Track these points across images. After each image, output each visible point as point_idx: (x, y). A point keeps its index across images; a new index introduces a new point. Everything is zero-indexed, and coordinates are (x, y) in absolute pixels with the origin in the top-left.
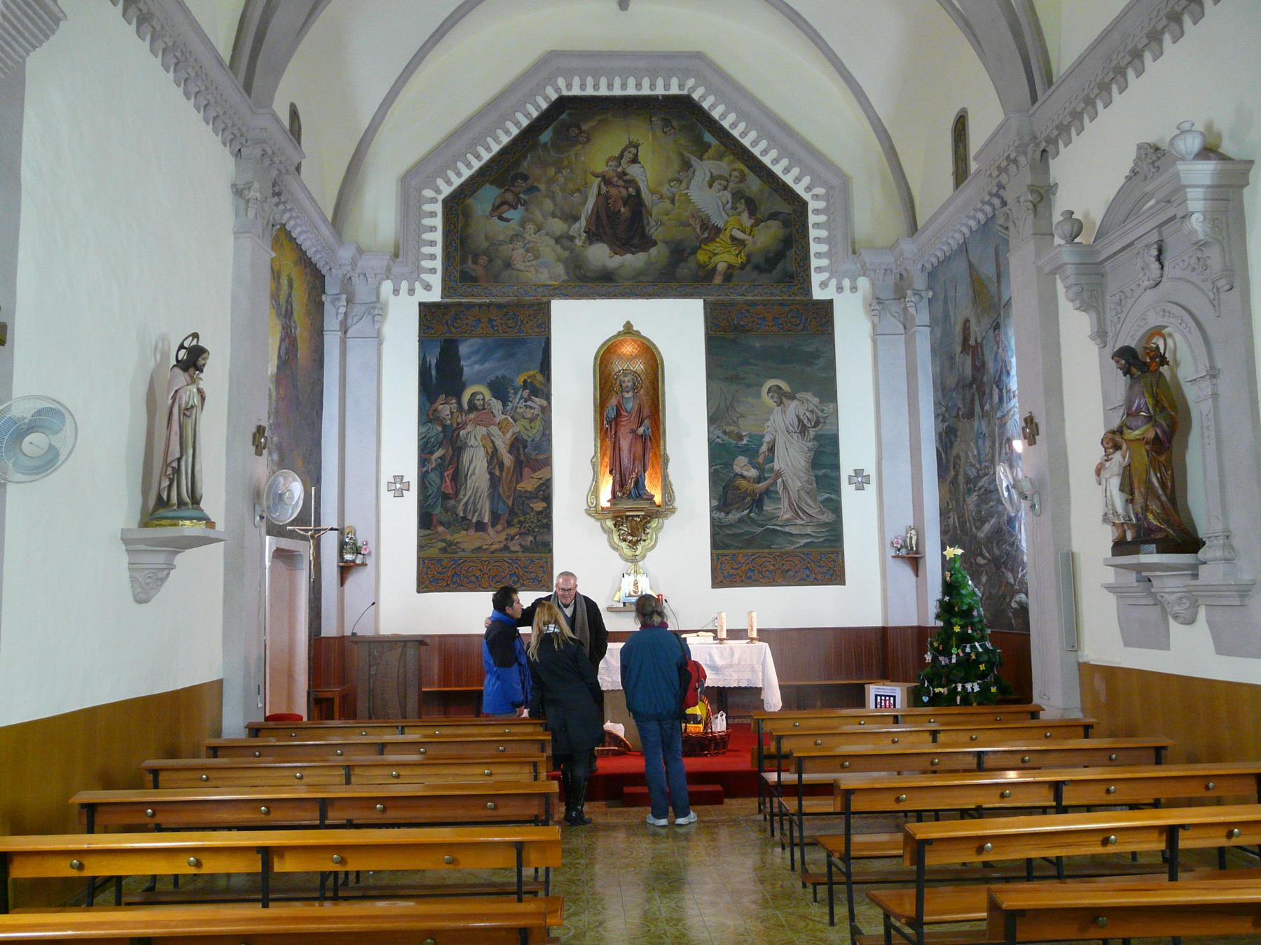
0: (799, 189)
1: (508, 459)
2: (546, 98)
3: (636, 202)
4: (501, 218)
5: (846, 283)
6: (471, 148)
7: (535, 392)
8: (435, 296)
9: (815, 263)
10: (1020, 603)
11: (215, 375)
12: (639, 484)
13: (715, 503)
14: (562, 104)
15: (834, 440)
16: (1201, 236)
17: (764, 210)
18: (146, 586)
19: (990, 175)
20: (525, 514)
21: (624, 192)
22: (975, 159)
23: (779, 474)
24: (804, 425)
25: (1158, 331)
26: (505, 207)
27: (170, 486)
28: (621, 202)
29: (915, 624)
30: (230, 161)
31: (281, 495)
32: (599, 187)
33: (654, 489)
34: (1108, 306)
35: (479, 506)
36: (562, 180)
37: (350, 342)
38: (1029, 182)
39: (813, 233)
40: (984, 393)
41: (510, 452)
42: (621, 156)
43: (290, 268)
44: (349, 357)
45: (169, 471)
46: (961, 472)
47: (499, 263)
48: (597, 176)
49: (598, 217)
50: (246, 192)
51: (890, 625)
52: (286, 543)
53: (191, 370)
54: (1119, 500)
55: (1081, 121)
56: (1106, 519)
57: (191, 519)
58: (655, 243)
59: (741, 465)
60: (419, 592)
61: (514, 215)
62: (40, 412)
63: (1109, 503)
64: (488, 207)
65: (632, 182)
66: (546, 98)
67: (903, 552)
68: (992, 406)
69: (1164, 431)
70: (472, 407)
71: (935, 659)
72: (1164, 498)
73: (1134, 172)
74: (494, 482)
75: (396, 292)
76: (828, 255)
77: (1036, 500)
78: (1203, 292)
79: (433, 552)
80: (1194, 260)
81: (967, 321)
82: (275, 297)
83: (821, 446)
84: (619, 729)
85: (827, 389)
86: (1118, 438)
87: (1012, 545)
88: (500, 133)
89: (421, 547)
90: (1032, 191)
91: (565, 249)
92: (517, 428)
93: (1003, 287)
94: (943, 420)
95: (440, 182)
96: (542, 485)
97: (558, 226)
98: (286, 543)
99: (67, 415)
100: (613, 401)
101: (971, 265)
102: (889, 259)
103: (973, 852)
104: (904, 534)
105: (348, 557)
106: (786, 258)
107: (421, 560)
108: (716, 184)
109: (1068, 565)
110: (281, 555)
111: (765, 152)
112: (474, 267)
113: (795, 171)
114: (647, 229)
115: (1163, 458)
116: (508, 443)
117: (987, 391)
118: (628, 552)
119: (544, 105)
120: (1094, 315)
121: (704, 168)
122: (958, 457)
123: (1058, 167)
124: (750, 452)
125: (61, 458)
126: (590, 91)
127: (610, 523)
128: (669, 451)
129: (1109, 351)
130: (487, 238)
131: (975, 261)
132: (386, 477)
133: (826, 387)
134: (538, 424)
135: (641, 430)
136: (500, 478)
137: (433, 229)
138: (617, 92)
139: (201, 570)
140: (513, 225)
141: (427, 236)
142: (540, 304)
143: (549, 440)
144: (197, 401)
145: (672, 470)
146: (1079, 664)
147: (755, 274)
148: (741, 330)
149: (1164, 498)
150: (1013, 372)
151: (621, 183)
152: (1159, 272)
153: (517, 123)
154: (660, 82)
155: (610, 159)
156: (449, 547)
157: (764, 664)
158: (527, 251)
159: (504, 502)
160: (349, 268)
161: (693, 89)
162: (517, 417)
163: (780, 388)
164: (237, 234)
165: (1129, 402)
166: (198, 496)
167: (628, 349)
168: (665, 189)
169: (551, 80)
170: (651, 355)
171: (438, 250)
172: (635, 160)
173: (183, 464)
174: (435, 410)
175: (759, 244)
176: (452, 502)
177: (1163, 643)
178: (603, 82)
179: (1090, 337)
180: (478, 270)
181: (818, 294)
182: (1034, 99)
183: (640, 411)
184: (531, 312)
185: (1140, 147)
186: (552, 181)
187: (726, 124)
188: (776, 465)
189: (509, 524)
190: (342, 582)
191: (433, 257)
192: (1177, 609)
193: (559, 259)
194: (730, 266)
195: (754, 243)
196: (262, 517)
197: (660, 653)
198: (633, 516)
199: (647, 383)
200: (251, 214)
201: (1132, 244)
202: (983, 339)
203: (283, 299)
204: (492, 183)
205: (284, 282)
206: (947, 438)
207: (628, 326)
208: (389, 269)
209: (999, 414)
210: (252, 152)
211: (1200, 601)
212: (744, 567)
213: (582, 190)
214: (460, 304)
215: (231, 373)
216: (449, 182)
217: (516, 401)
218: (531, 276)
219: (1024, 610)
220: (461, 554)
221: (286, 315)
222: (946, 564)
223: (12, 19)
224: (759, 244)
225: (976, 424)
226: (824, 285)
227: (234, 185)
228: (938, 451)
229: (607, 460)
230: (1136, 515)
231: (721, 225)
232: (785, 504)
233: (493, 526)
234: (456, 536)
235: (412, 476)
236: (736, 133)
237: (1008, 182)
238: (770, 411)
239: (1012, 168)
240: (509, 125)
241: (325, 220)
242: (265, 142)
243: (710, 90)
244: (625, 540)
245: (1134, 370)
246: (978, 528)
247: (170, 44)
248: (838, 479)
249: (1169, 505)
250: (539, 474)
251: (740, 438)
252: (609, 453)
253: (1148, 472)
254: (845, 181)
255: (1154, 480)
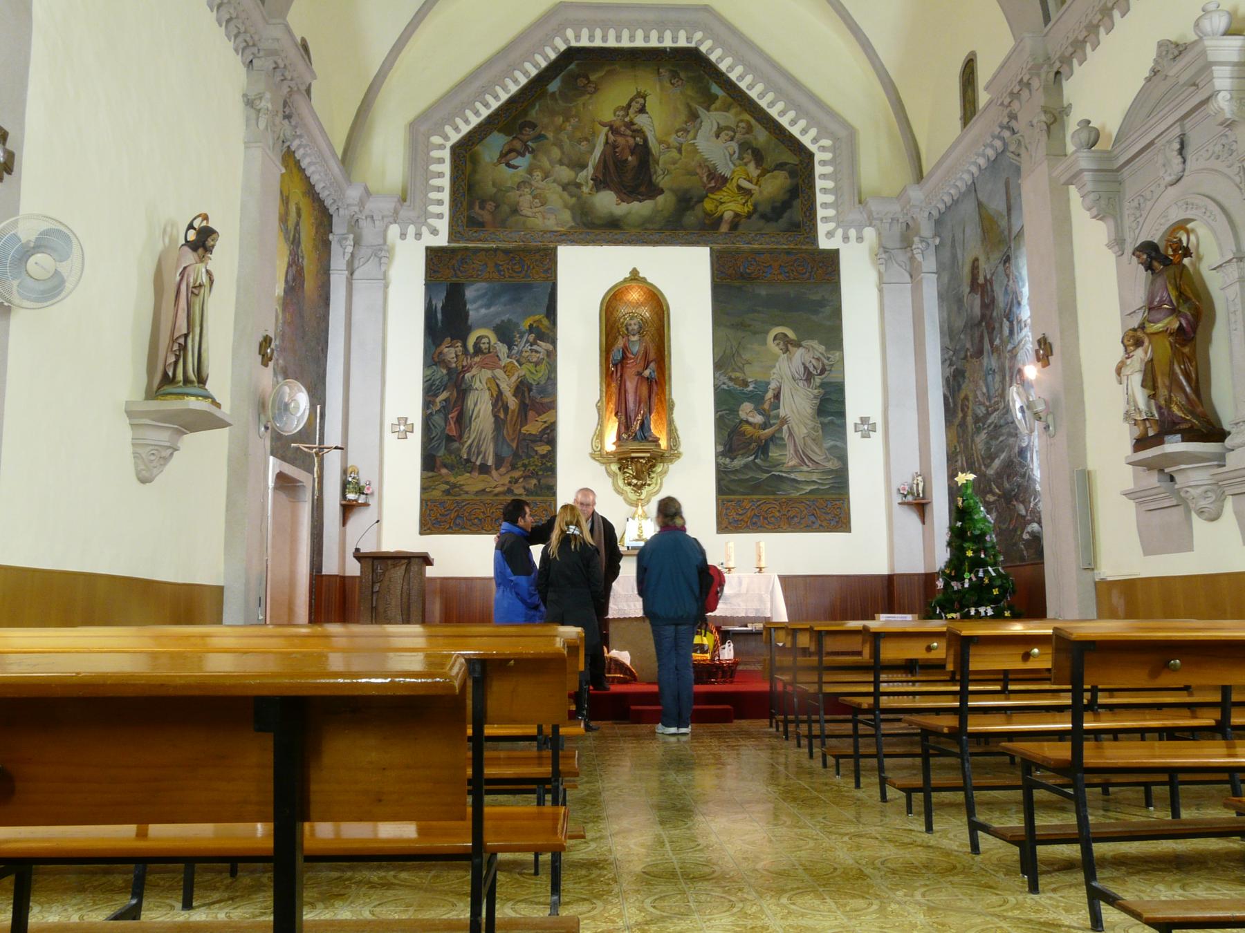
0: (806, 140)
2: (555, 49)
3: (643, 152)
4: (508, 165)
5: (852, 233)
6: (479, 97)
8: (442, 240)
9: (821, 213)
10: (1032, 534)
11: (225, 259)
12: (644, 426)
13: (721, 449)
14: (571, 54)
16: (1228, 116)
17: (770, 161)
18: (148, 468)
21: (631, 141)
22: (986, 89)
23: (784, 421)
25: (1182, 225)
26: (513, 154)
27: (176, 363)
28: (627, 151)
30: (242, 70)
31: (286, 405)
32: (607, 135)
33: (658, 430)
34: (1126, 212)
35: (483, 449)
36: (569, 128)
37: (356, 284)
38: (1042, 102)
39: (819, 184)
40: (994, 328)
41: (515, 395)
42: (629, 106)
43: (297, 196)
44: (355, 299)
45: (176, 347)
46: (970, 412)
47: (505, 208)
48: (604, 125)
49: (605, 166)
50: (257, 102)
51: (897, 572)
52: (290, 470)
53: (201, 251)
54: (1140, 396)
55: (1097, 34)
56: (1127, 416)
58: (661, 192)
59: (746, 411)
60: (421, 534)
61: (522, 162)
62: (47, 232)
63: (1130, 400)
64: (496, 155)
65: (640, 132)
66: (555, 49)
67: (910, 498)
69: (1188, 322)
70: (478, 350)
71: (947, 585)
72: (1188, 389)
73: (1155, 72)
74: (499, 424)
75: (403, 236)
76: (834, 205)
78: (1229, 177)
79: (437, 494)
81: (976, 260)
82: (284, 219)
83: (826, 393)
84: (625, 657)
85: (833, 337)
86: (1140, 334)
87: (1023, 476)
88: (508, 81)
89: (424, 489)
90: (1045, 112)
91: (572, 196)
92: (523, 371)
93: (1013, 220)
95: (448, 129)
97: (565, 173)
98: (290, 470)
99: (74, 240)
101: (980, 205)
102: (896, 208)
103: (1020, 658)
104: (910, 481)
105: (351, 496)
108: (723, 135)
109: (1084, 483)
110: (284, 482)
111: (772, 104)
113: (802, 123)
115: (1186, 350)
116: (513, 386)
117: (997, 325)
118: (633, 496)
119: (553, 56)
121: (711, 119)
122: (966, 398)
123: (1071, 89)
124: (756, 398)
125: (69, 285)
126: (598, 43)
127: (614, 467)
128: (674, 397)
130: (494, 185)
131: (983, 199)
132: (390, 419)
133: (831, 334)
134: (543, 368)
135: (647, 373)
136: (504, 421)
137: (440, 175)
138: (625, 43)
139: (205, 454)
140: (521, 172)
141: (435, 182)
143: (554, 384)
144: (205, 279)
145: (677, 415)
146: (1096, 583)
147: (762, 223)
149: (1188, 389)
150: (1025, 302)
151: (628, 132)
152: (1181, 166)
153: (525, 73)
154: (668, 35)
156: (452, 490)
157: (772, 593)
158: (535, 197)
159: (509, 445)
160: (356, 209)
161: (701, 42)
162: (523, 360)
163: (786, 335)
164: (248, 144)
166: (204, 375)
167: (635, 295)
168: (672, 139)
169: (560, 31)
170: (657, 301)
171: (445, 196)
172: (642, 110)
174: (441, 353)
175: (765, 193)
176: (456, 445)
177: (1184, 543)
178: (612, 34)
180: (485, 216)
181: (824, 243)
182: (1047, 18)
183: (646, 353)
184: (537, 256)
185: (1161, 45)
186: (560, 129)
187: (733, 76)
189: (513, 467)
190: (344, 523)
191: (440, 202)
192: (1203, 503)
193: (566, 206)
194: (737, 215)
195: (761, 192)
196: (267, 428)
198: (639, 458)
200: (262, 125)
201: (1151, 143)
202: (992, 275)
204: (499, 131)
206: (954, 382)
207: (635, 272)
208: (396, 212)
209: (1010, 347)
211: (1228, 491)
212: (749, 514)
213: (590, 140)
214: (467, 249)
215: (229, 460)
217: (522, 345)
219: (1037, 540)
221: (295, 243)
222: (954, 491)
224: (765, 193)
225: (985, 361)
226: (830, 234)
227: (245, 95)
228: (945, 398)
231: (728, 174)
232: (790, 451)
233: (497, 469)
234: (459, 478)
235: (416, 418)
236: (742, 85)
237: (1015, 110)
238: (776, 358)
240: (518, 74)
241: (334, 154)
243: (718, 42)
244: (629, 484)
245: (1155, 264)
246: (987, 466)
248: (843, 426)
250: (544, 417)
251: (746, 384)
252: (614, 399)
254: (852, 133)
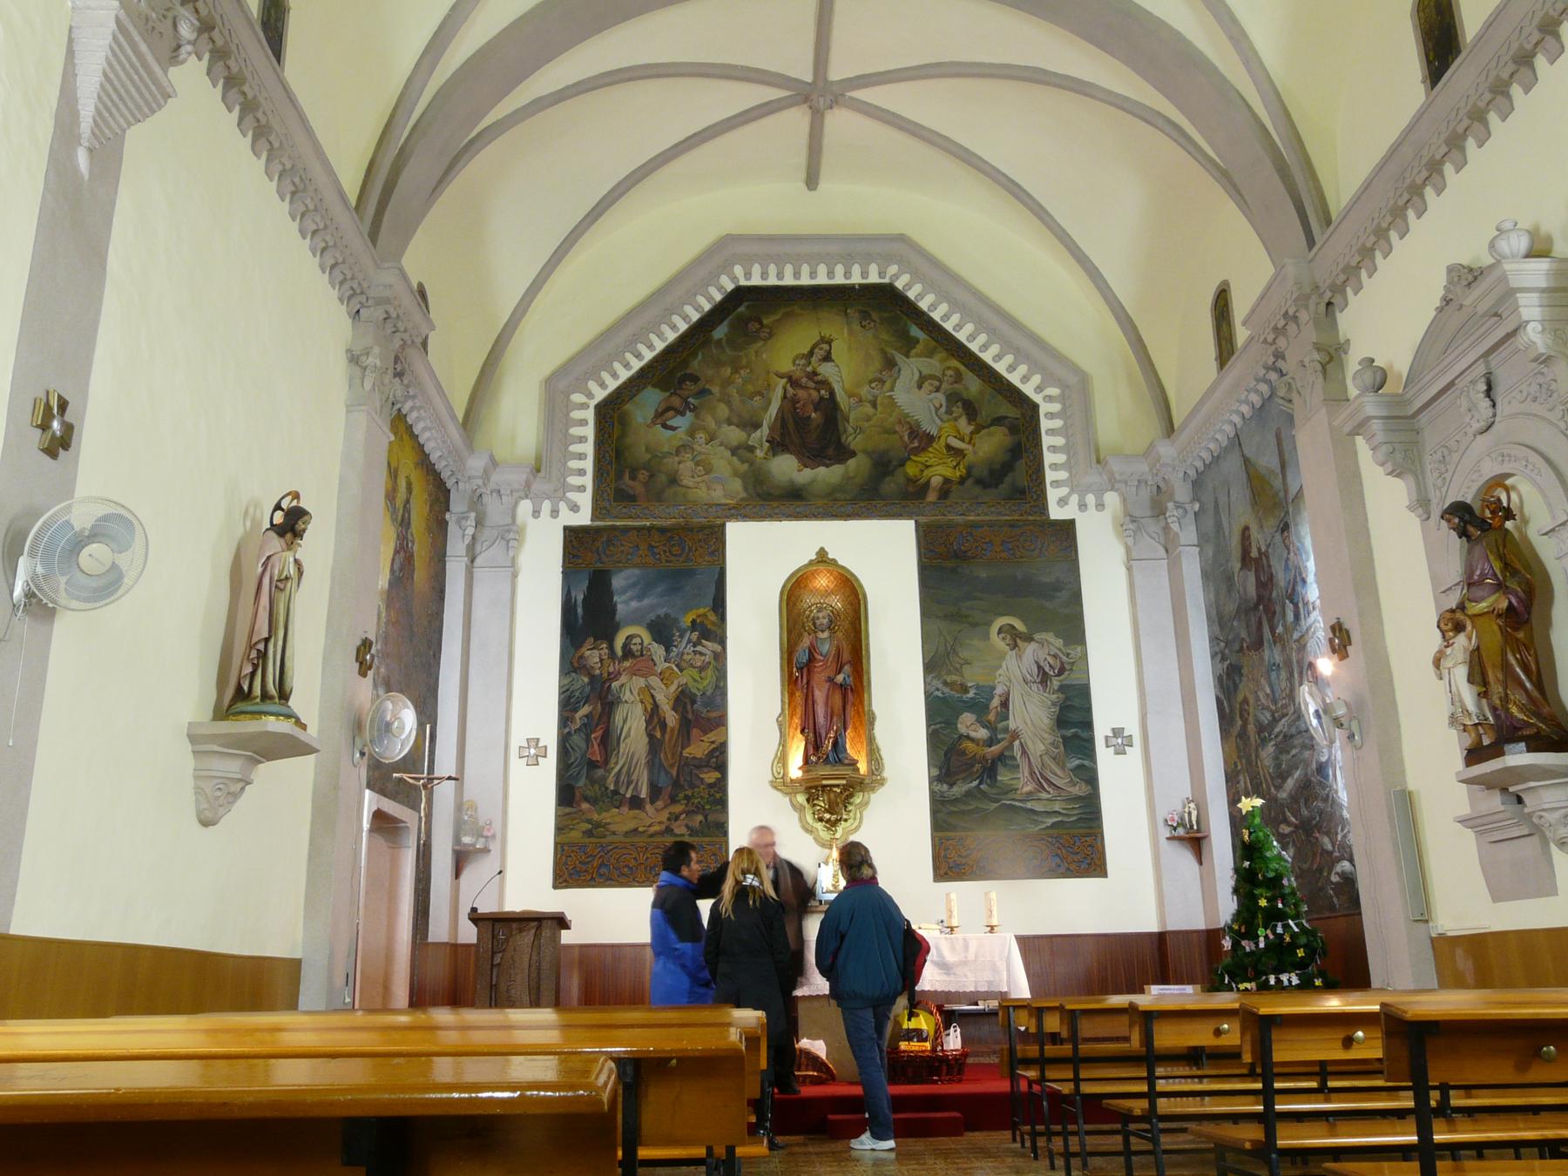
0: (1028, 390)
1: (672, 718)
3: (829, 406)
4: (665, 426)
5: (1091, 499)
7: (706, 634)
8: (584, 518)
9: (1050, 476)
10: (1343, 875)
13: (936, 772)
15: (1084, 692)
17: (984, 415)
19: (1265, 341)
20: (692, 786)
21: (815, 394)
22: (1244, 323)
23: (1015, 735)
24: (1045, 673)
25: (1499, 481)
26: (671, 413)
27: (253, 674)
29: (1203, 927)
30: (347, 322)
31: (388, 725)
34: (1428, 467)
35: (634, 777)
37: (478, 573)
41: (674, 709)
42: (811, 353)
43: (408, 468)
44: (477, 591)
45: (254, 654)
46: (1251, 719)
47: (663, 478)
50: (363, 358)
51: (1170, 928)
52: (391, 807)
53: (289, 536)
54: (1468, 695)
55: (1373, 259)
56: (1453, 720)
57: (277, 715)
59: (967, 723)
60: (555, 887)
61: (682, 422)
62: (106, 518)
63: (1455, 699)
65: (825, 384)
66: (720, 288)
67: (1181, 832)
68: (1285, 626)
70: (628, 653)
71: (1236, 945)
72: (1528, 685)
73: (1447, 301)
74: (654, 745)
75: (536, 513)
76: (1067, 466)
77: (1355, 727)
78: (1551, 423)
79: (575, 835)
80: (1534, 388)
81: (1246, 529)
82: (391, 496)
83: (1067, 699)
84: (819, 1048)
85: (1072, 628)
86: (1459, 615)
87: (1326, 800)
88: (665, 328)
89: (560, 829)
90: (1318, 350)
94: (1223, 659)
95: (592, 386)
96: (714, 750)
97: (735, 435)
98: (391, 807)
100: (806, 641)
101: (1246, 461)
104: (1180, 808)
105: (466, 840)
106: (1015, 469)
107: (559, 846)
109: (1405, 806)
110: (381, 820)
112: (631, 483)
114: (843, 438)
115: (1521, 635)
116: (673, 697)
117: (1278, 609)
118: (825, 835)
120: (1411, 479)
121: (911, 368)
122: (1245, 701)
123: (1346, 322)
124: (979, 707)
126: (772, 281)
127: (801, 799)
128: (874, 708)
129: (1436, 512)
130: (648, 449)
132: (517, 740)
135: (840, 678)
136: (661, 742)
138: (805, 281)
140: (681, 434)
142: (711, 527)
144: (292, 570)
145: (879, 731)
146: (1432, 939)
147: (977, 490)
148: (961, 556)
149: (1528, 685)
150: (1311, 578)
151: (811, 384)
152: (1490, 412)
153: (685, 318)
155: (796, 358)
156: (596, 829)
158: (697, 464)
159: (667, 773)
160: (480, 482)
161: (896, 276)
162: (684, 664)
165: (1469, 571)
167: (823, 581)
168: (865, 391)
169: (726, 268)
171: (588, 464)
172: (827, 358)
173: (271, 646)
174: (581, 657)
176: (600, 772)
177: (1545, 885)
179: (1409, 508)
180: (637, 487)
181: (1056, 513)
182: (1311, 242)
184: (701, 536)
186: (727, 383)
187: (936, 316)
188: (1012, 724)
189: (673, 800)
190: (457, 875)
191: (582, 472)
193: (736, 474)
194: (947, 481)
196: (362, 754)
197: (877, 944)
198: (832, 785)
199: (846, 624)
200: (368, 385)
201: (1451, 384)
203: (399, 502)
204: (654, 386)
205: (402, 483)
206: (1229, 682)
207: (822, 553)
208: (528, 485)
209: (1296, 635)
210: (374, 313)
213: (764, 394)
214: (614, 528)
216: (603, 385)
217: (682, 646)
218: (701, 494)
219: (1349, 882)
220: (611, 838)
221: (404, 523)
222: (1238, 821)
223: (116, 83)
225: (1266, 653)
226: (1063, 502)
227: (348, 351)
229: (797, 721)
230: (1494, 709)
231: (934, 432)
232: (1024, 772)
233: (652, 802)
234: (605, 814)
236: (948, 326)
237: (1282, 351)
238: (1002, 657)
239: (1292, 328)
241: (454, 417)
242: (387, 301)
243: (917, 276)
244: (821, 820)
245: (1471, 529)
246: (1278, 788)
247: (288, 166)
248: (1091, 741)
249: (1536, 694)
250: (711, 736)
251: (965, 690)
252: (799, 711)
253: (1504, 654)
254: (1084, 379)
255: (1513, 662)
